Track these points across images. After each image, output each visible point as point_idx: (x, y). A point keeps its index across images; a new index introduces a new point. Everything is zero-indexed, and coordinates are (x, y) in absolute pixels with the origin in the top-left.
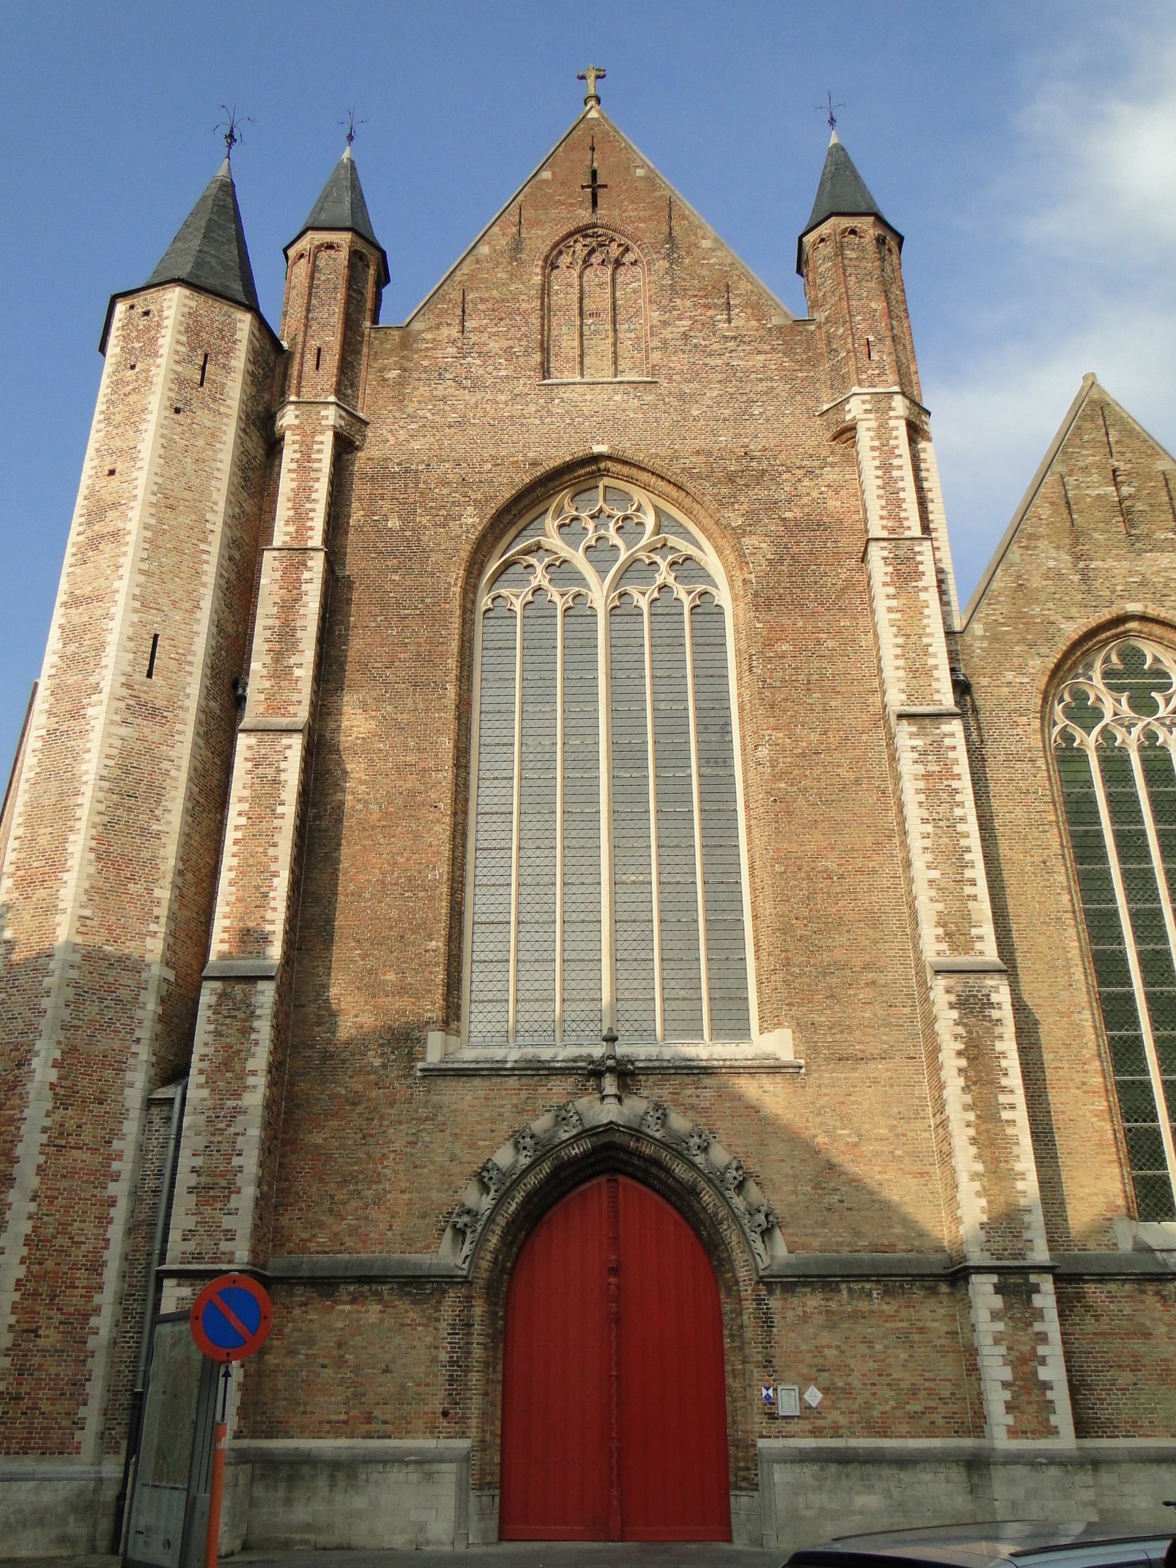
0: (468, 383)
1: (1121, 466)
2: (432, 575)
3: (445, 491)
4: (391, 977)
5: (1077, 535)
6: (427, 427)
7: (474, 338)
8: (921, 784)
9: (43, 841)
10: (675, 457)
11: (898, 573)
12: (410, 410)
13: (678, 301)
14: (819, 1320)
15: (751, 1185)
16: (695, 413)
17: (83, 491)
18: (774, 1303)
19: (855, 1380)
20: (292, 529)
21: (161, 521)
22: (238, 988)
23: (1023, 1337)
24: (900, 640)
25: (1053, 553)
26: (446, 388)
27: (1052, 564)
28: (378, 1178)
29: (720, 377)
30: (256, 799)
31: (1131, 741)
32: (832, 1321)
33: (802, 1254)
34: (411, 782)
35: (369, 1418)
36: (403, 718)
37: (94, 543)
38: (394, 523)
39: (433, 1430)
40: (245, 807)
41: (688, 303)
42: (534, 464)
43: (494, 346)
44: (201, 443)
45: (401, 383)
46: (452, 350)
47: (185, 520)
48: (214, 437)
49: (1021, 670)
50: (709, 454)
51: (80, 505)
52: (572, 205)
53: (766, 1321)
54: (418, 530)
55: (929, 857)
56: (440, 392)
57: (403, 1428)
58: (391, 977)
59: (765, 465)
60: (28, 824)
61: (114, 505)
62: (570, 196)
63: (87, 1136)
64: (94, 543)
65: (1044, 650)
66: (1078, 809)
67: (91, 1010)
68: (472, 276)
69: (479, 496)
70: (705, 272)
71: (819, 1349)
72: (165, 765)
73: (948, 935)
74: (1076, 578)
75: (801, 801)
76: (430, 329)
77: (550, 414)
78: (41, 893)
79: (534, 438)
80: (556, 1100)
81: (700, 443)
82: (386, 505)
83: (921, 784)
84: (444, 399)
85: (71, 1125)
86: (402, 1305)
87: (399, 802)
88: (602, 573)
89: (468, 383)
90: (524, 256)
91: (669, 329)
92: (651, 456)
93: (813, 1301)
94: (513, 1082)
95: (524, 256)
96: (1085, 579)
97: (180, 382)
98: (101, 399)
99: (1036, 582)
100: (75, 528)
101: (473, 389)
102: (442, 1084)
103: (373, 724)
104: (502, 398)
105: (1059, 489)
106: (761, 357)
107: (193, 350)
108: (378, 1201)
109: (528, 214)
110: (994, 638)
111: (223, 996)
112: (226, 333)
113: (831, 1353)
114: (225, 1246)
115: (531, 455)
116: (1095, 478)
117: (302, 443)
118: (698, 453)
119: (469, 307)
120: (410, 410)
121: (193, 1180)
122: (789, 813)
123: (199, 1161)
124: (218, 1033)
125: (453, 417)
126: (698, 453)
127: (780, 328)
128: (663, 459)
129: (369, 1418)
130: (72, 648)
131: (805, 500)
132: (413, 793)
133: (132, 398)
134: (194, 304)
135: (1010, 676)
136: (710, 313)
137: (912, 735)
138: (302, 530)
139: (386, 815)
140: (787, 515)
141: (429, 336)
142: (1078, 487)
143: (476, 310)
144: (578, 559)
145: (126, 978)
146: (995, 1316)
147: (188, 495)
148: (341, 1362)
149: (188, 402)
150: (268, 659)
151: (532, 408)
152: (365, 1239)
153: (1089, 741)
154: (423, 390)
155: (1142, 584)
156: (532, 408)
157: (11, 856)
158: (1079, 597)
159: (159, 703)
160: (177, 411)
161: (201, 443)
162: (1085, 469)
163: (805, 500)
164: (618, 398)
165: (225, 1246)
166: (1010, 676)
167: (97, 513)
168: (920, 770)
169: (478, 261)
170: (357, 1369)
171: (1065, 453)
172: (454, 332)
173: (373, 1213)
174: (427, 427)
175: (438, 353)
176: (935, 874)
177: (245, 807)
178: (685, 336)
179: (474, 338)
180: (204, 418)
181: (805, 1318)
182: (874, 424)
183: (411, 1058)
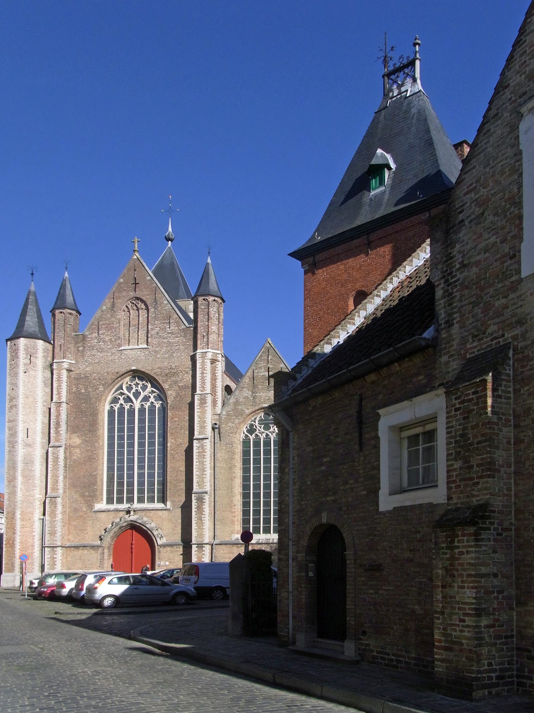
0: (100, 350)
1: (271, 366)
2: (92, 404)
3: (95, 382)
4: (87, 494)
5: (254, 386)
6: (91, 364)
7: (102, 336)
8: (197, 454)
9: (11, 473)
10: (152, 370)
11: (201, 403)
12: (86, 359)
13: (156, 322)
14: (170, 552)
15: (159, 530)
16: (159, 356)
17: (7, 394)
18: (161, 549)
19: (176, 561)
20: (57, 396)
21: (25, 402)
22: (53, 499)
23: (200, 555)
24: (199, 420)
25: (247, 392)
26: (94, 352)
27: (246, 395)
28: (87, 530)
29: (166, 345)
30: (54, 461)
31: (262, 437)
32: (172, 552)
33: (169, 541)
34: (90, 453)
35: (86, 567)
36: (87, 439)
37: (11, 407)
38: (83, 391)
39: (97, 569)
40: (52, 463)
41: (159, 322)
42: (117, 373)
43: (107, 339)
44: (32, 379)
45: (83, 351)
46: (96, 341)
47: (31, 400)
48: (35, 377)
49: (233, 423)
50: (161, 368)
51: (8, 397)
52: (128, 291)
53: (160, 552)
54: (89, 392)
55: (197, 470)
56: (93, 353)
57: (92, 568)
58: (87, 494)
59: (175, 371)
60: (8, 469)
61: (14, 398)
62: (128, 288)
63: (28, 525)
64: (11, 407)
65: (240, 418)
66: (246, 453)
67: (25, 504)
68: (101, 317)
69: (103, 382)
70: (164, 312)
71: (169, 557)
72: (33, 456)
73: (199, 485)
74: (251, 398)
75: (176, 455)
76: (90, 334)
77: (121, 358)
78: (12, 484)
79: (117, 366)
80: (121, 516)
81: (159, 365)
82: (81, 386)
83: (197, 454)
84: (94, 355)
85: (25, 524)
86: (91, 550)
87: (87, 458)
88: (137, 399)
89: (100, 350)
90: (115, 309)
91: (154, 331)
92: (146, 370)
93: (169, 549)
94: (112, 513)
95: (115, 309)
96: (254, 398)
97: (25, 364)
98: (8, 369)
99: (241, 400)
100: (7, 403)
101: (101, 352)
102: (98, 513)
103: (81, 441)
104: (109, 354)
105: (252, 374)
106: (178, 339)
107: (27, 355)
108: (87, 534)
109: (116, 294)
110: (228, 415)
111: (50, 500)
112: (35, 347)
113: (171, 557)
114: (55, 542)
115: (116, 371)
116: (263, 370)
117: (58, 373)
118: (158, 368)
119: (100, 326)
120: (86, 359)
121: (48, 532)
122: (173, 458)
123: (49, 529)
124: (50, 507)
125: (97, 361)
126: (158, 368)
127: (183, 329)
128: (149, 370)
129: (86, 567)
130: (11, 432)
131: (185, 380)
132: (90, 456)
133: (14, 370)
134: (25, 342)
135: (230, 424)
136: (165, 325)
137: (197, 443)
138: (59, 398)
139: (84, 461)
140: (180, 385)
141: (89, 336)
142: (257, 373)
143: (102, 327)
144: (131, 396)
145: (31, 498)
146: (195, 551)
147: (30, 394)
148: (81, 559)
149: (27, 369)
150: (54, 429)
151: (117, 357)
152: (85, 540)
153: (252, 437)
154: (89, 353)
155: (268, 399)
156: (117, 357)
157: (6, 476)
158: (251, 403)
159: (30, 443)
160: (25, 372)
161: (32, 379)
162: (260, 368)
163: (185, 380)
164: (139, 353)
165: (55, 542)
166: (230, 424)
167: (11, 400)
168: (198, 451)
169: (102, 312)
170: (83, 560)
171: (256, 363)
172: (96, 335)
173: (86, 536)
174: (91, 364)
175: (92, 342)
176: (198, 473)
177: (52, 463)
178: (158, 333)
179: (102, 336)
180: (32, 372)
181: (167, 552)
182: (201, 361)
183: (92, 509)
